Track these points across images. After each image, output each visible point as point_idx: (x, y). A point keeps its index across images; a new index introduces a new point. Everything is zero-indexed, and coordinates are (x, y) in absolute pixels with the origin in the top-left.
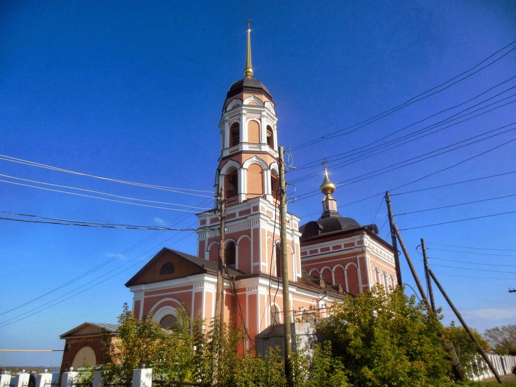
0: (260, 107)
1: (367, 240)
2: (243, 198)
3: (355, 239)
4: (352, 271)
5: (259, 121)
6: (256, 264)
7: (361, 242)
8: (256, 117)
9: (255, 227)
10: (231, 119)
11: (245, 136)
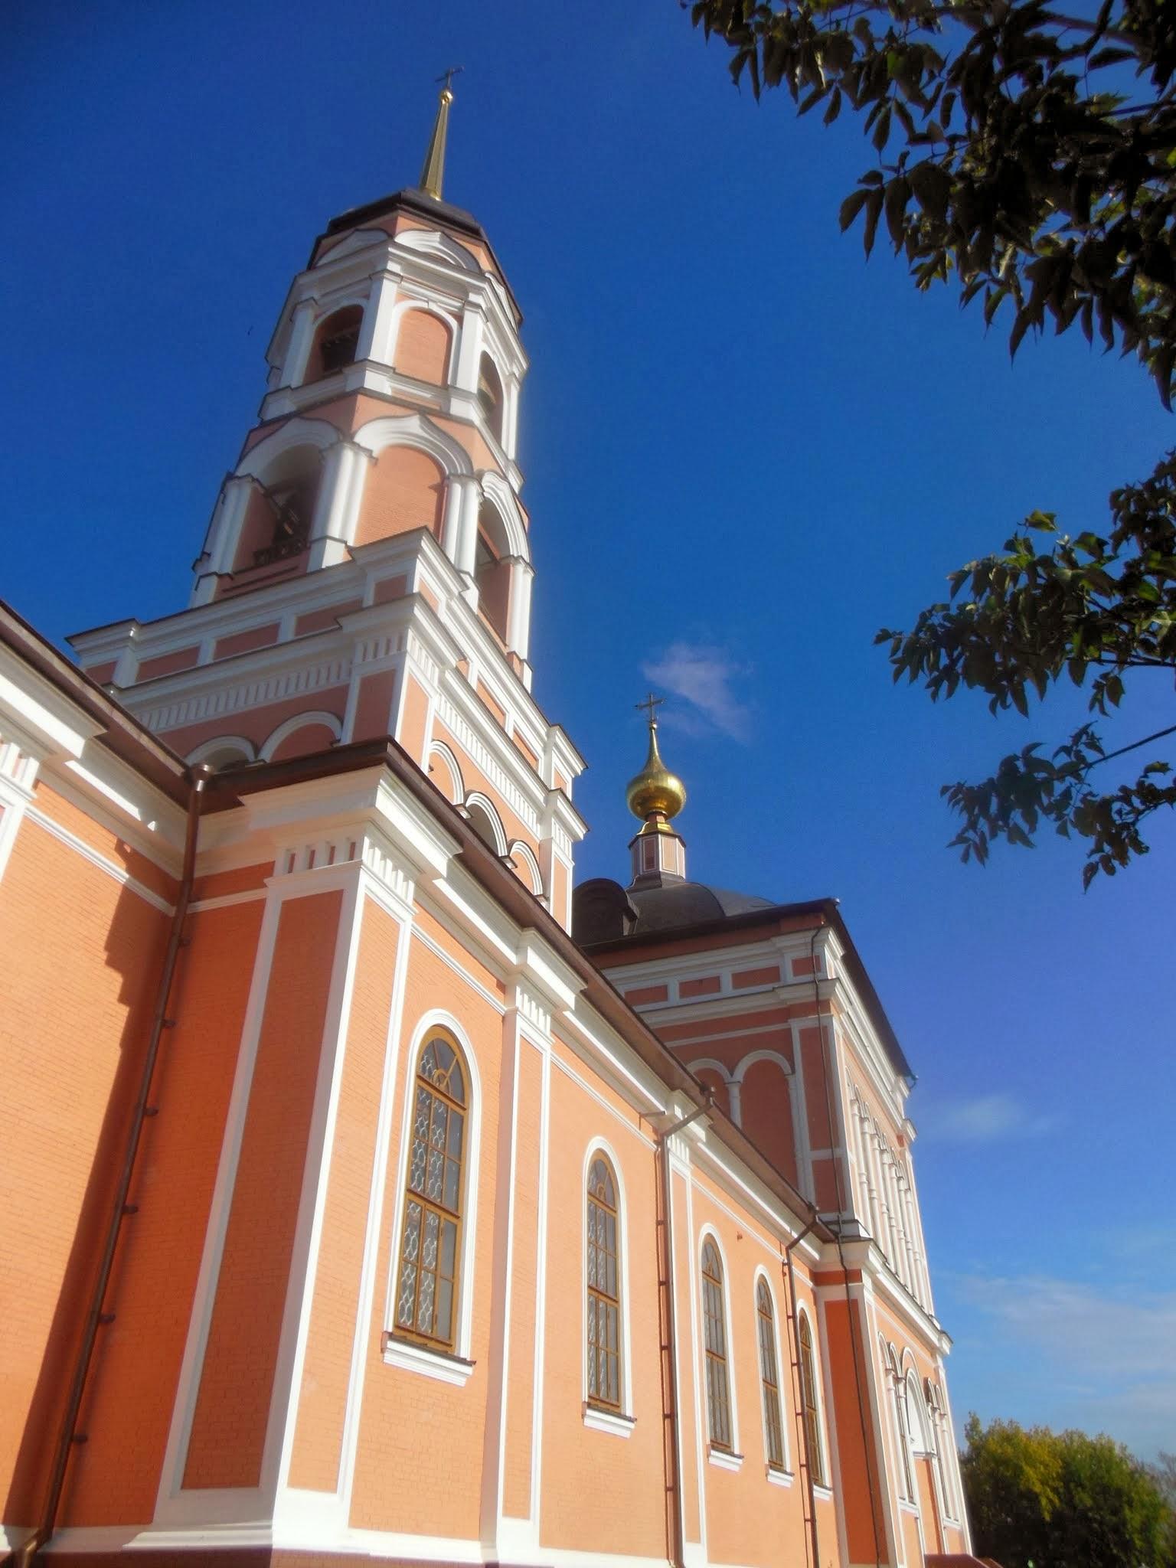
2: (333, 555)
3: (789, 947)
5: (453, 323)
8: (442, 304)
9: (371, 669)
10: (327, 300)
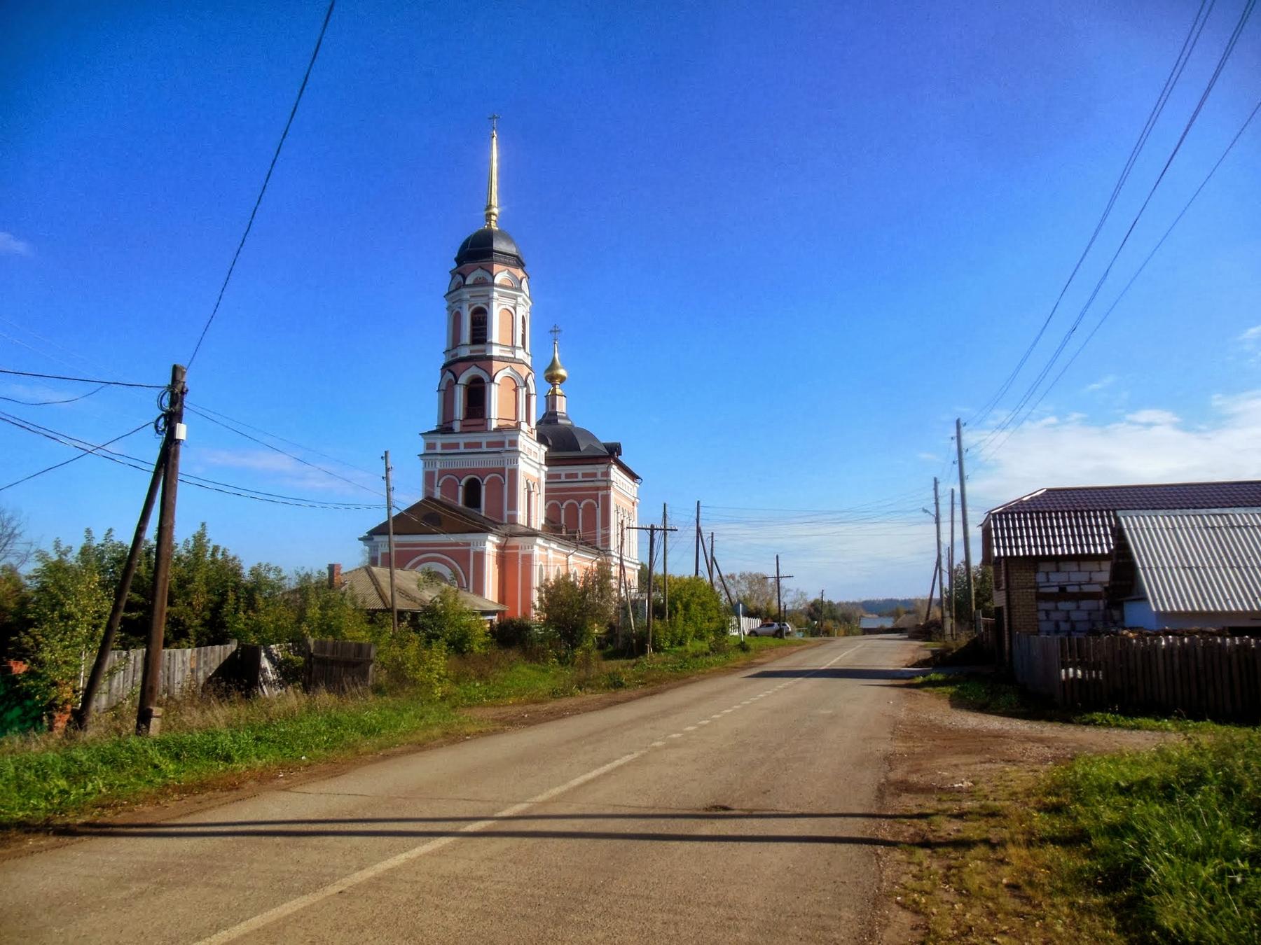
0: (516, 289)
1: (615, 473)
3: (600, 469)
4: (590, 510)
6: (511, 512)
7: (607, 474)
8: (509, 303)
11: (496, 332)
